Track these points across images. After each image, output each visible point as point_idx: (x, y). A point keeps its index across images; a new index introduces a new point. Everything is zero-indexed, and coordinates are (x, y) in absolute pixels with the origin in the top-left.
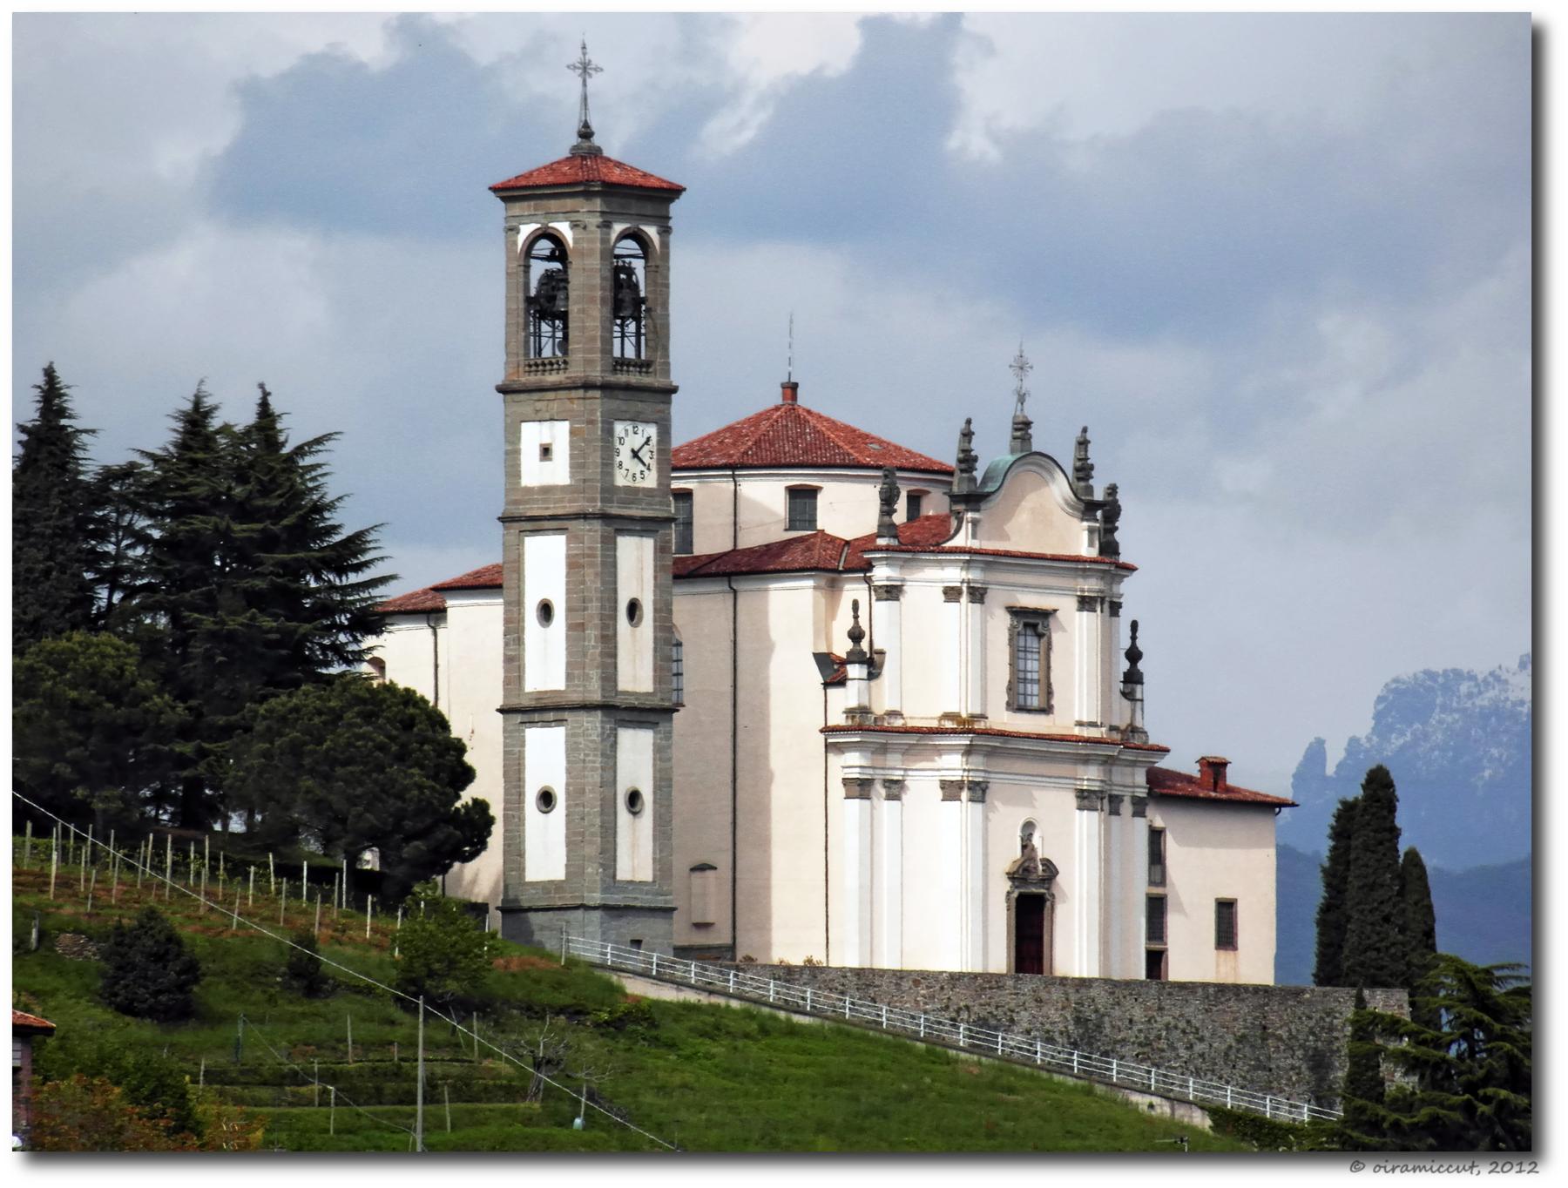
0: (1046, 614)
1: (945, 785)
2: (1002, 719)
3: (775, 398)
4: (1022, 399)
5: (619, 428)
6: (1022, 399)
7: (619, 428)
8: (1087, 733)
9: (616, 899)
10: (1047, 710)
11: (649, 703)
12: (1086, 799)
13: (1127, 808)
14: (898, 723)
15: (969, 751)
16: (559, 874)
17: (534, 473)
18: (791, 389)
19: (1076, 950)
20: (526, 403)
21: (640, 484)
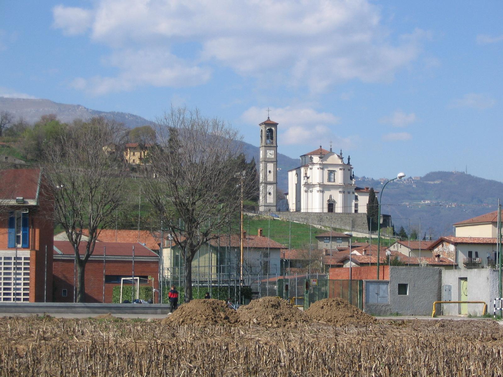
0: (334, 171)
1: (339, 191)
2: (326, 182)
3: (319, 148)
4: (331, 146)
5: (268, 151)
6: (331, 146)
7: (268, 151)
8: (340, 184)
9: (267, 205)
10: (334, 181)
11: (273, 182)
12: (340, 192)
13: (351, 193)
14: (312, 184)
15: (320, 187)
16: (336, 212)
17: (269, 156)
18: (321, 147)
19: (339, 209)
20: (267, 148)
21: (271, 157)
